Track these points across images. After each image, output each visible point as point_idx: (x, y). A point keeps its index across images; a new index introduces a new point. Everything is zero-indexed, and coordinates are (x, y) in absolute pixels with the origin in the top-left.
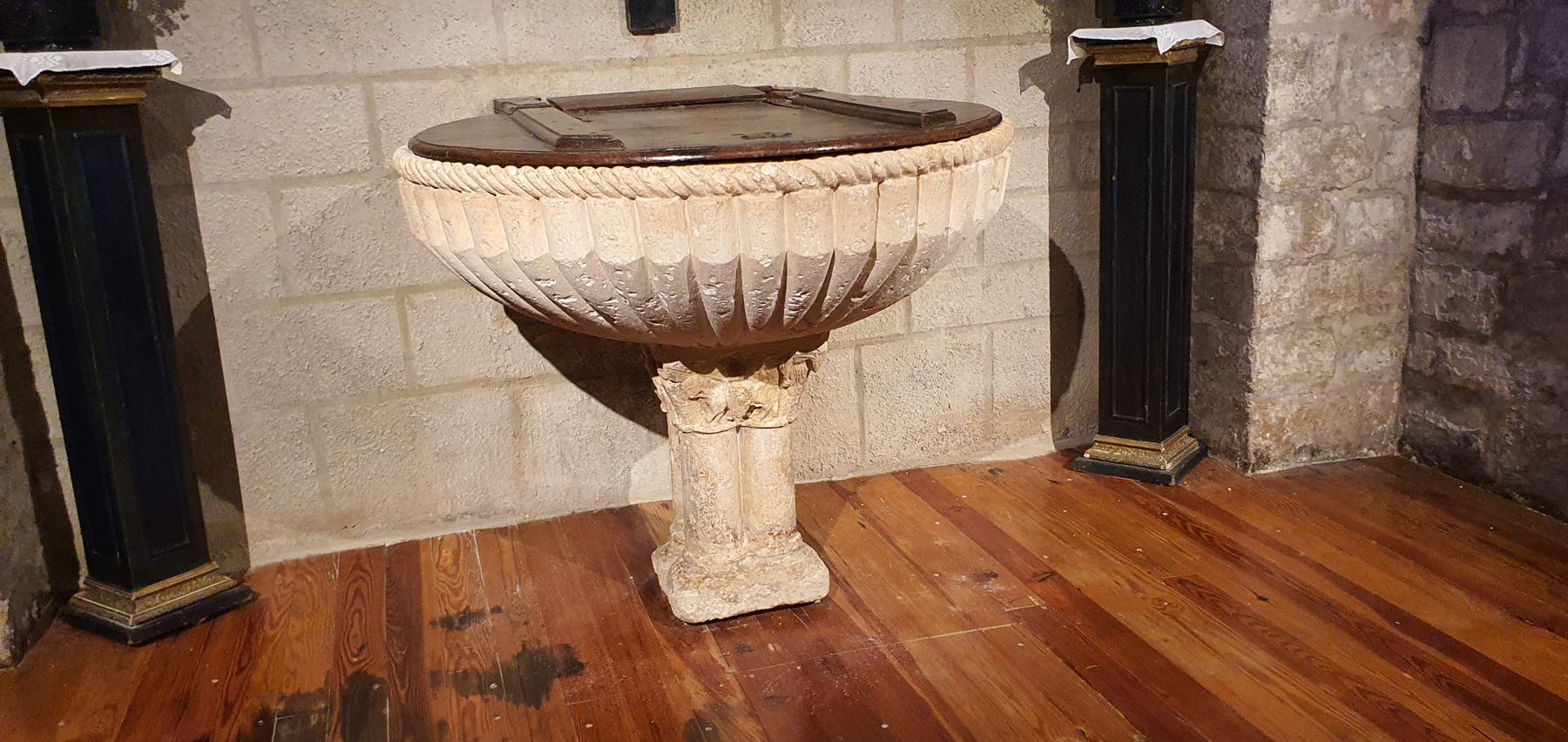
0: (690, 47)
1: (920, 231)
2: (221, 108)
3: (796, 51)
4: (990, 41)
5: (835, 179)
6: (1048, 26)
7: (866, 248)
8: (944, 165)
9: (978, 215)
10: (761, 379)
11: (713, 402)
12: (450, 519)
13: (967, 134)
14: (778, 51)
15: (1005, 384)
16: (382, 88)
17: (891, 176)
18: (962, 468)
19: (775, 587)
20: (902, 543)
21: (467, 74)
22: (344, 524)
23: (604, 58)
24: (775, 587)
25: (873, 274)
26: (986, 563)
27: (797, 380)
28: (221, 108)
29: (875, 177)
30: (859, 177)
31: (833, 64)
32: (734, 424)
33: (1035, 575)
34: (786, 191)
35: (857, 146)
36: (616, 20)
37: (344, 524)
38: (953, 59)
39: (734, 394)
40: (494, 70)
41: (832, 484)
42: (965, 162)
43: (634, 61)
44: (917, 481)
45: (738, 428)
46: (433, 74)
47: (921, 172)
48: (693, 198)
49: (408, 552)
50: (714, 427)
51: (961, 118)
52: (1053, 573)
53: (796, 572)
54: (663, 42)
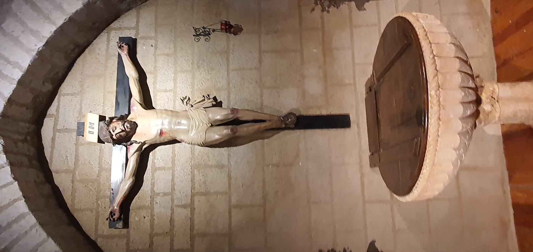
0: (354, 111)
2: (372, 244)
3: (354, 79)
4: (351, 19)
5: (436, 71)
6: (346, 3)
7: (458, 60)
8: (426, 35)
11: (490, 110)
12: (505, 192)
14: (355, 85)
16: (366, 198)
18: (494, 23)
21: (362, 175)
22: (504, 225)
25: (463, 58)
27: (482, 82)
28: (372, 244)
29: (434, 58)
32: (497, 103)
34: (439, 87)
35: (423, 64)
37: (504, 225)
40: (361, 167)
41: (498, 68)
43: (358, 125)
44: (498, 39)
45: (497, 101)
46: (363, 184)
49: (516, 206)
50: (498, 110)
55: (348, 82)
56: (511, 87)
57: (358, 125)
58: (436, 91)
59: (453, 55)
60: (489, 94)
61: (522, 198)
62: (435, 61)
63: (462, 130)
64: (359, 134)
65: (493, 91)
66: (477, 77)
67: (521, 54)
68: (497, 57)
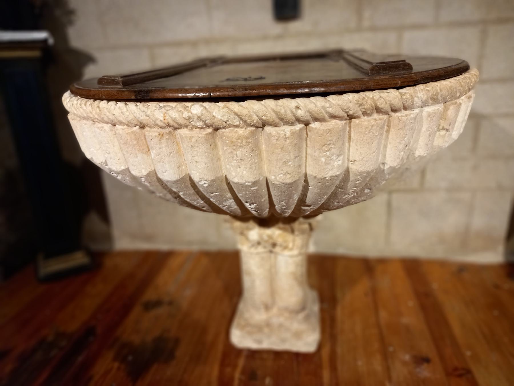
1: (353, 167)
8: (378, 110)
9: (420, 151)
10: (280, 229)
13: (414, 83)
14: (359, 29)
15: (479, 222)
17: (316, 119)
18: (442, 264)
19: (284, 341)
20: (383, 315)
22: (149, 238)
23: (258, 34)
24: (284, 341)
26: (426, 348)
29: (299, 120)
30: (282, 119)
31: (392, 37)
33: (456, 369)
36: (263, 15)
37: (149, 238)
38: (472, 34)
39: (261, 236)
42: (405, 108)
44: (413, 267)
47: (351, 117)
48: (147, 129)
49: (168, 255)
51: (417, 67)
52: (469, 372)
53: (298, 335)
54: (294, 26)
55: (367, 14)
56: (294, 274)
57: (279, 37)
58: (199, 118)
59: (311, 171)
60: (280, 241)
61: (174, 263)
62: (292, 124)
63: (118, 173)
64: (265, 38)
65: (286, 248)
66: (310, 225)
67: (374, 292)
68: (383, 261)
